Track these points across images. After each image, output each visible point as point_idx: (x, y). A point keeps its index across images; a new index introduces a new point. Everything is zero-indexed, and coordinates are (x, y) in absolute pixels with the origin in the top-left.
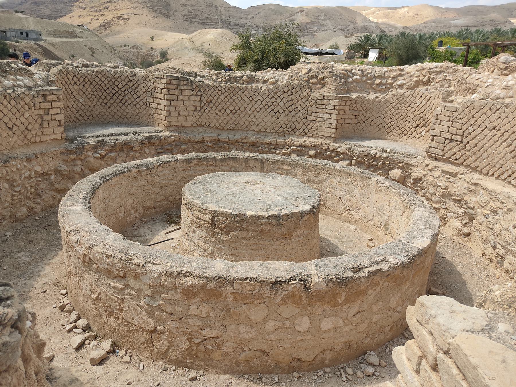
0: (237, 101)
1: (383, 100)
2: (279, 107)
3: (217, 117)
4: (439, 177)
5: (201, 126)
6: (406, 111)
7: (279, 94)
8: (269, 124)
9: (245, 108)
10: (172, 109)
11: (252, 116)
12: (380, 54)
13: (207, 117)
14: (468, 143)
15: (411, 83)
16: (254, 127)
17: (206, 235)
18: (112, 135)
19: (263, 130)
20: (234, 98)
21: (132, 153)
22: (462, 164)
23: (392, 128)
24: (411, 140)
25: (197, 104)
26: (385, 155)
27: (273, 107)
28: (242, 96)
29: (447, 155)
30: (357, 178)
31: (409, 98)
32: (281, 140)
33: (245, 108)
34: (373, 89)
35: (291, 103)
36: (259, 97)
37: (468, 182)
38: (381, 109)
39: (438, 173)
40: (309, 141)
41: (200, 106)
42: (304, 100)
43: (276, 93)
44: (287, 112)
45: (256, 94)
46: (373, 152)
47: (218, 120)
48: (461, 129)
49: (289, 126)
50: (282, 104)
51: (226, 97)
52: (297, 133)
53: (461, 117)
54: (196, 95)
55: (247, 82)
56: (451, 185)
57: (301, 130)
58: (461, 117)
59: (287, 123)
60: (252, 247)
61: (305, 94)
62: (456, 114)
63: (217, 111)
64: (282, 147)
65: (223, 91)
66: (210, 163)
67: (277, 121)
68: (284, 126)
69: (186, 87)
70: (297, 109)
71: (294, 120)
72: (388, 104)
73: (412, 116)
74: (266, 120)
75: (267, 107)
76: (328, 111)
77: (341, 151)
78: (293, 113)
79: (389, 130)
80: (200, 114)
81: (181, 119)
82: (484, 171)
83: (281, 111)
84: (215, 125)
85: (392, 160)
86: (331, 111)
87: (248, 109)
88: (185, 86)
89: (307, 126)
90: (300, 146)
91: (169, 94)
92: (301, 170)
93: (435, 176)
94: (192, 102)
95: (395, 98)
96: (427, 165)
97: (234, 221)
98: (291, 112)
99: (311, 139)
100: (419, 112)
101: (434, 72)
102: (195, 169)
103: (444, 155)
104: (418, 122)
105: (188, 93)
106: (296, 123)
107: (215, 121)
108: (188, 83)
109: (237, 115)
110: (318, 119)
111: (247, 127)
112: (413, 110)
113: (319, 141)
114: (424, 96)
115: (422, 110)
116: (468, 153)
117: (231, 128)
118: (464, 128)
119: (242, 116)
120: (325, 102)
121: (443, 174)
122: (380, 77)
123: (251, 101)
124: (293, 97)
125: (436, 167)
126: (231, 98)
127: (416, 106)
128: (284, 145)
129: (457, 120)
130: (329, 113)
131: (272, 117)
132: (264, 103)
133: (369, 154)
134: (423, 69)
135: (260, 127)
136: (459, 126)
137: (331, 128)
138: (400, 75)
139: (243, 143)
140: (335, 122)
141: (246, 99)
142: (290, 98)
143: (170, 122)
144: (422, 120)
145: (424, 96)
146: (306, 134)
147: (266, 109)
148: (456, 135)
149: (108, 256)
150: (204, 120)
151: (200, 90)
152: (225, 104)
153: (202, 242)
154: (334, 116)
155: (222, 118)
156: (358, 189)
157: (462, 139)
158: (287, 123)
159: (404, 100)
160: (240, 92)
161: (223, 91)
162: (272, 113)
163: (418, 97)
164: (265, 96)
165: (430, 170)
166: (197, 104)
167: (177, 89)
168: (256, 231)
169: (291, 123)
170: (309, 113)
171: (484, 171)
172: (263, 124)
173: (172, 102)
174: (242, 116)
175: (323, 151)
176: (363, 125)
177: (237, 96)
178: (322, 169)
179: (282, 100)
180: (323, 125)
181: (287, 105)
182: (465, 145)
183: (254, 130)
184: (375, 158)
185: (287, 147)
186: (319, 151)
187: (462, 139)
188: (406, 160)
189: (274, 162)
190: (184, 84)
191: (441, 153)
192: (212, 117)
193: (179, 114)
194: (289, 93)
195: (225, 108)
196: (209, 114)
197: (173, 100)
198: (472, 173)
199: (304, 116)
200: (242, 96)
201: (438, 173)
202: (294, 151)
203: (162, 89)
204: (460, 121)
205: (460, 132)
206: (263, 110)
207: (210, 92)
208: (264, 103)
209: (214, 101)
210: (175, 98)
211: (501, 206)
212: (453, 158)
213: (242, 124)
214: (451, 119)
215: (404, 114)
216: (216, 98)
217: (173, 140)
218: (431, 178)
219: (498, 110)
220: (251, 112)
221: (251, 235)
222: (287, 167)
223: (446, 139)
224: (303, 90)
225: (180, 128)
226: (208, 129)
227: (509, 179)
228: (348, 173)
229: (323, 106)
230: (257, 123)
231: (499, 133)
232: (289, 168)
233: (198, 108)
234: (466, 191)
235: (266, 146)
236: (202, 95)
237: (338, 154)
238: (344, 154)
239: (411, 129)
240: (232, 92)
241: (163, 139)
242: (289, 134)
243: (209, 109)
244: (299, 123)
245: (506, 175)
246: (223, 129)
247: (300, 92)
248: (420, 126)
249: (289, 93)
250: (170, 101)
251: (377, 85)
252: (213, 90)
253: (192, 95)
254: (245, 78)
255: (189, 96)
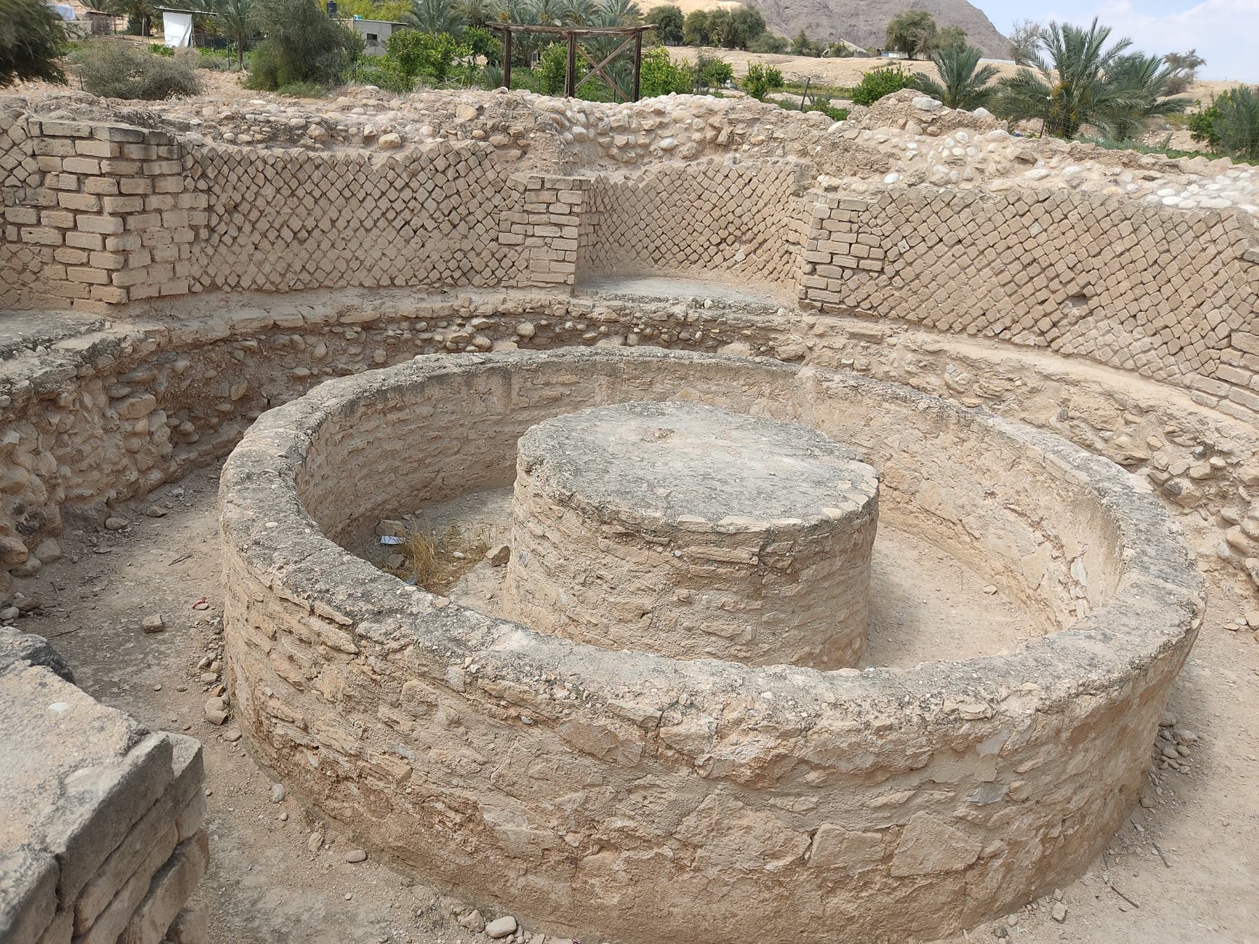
0: (309, 201)
1: (641, 186)
2: (424, 214)
3: (258, 256)
4: (844, 346)
5: (214, 287)
6: (693, 210)
7: (422, 177)
8: (400, 262)
9: (333, 222)
10: (132, 242)
11: (353, 245)
12: (197, 28)
13: (231, 259)
14: (897, 273)
15: (689, 144)
16: (362, 275)
17: (735, 598)
18: (1063, 380)
19: (385, 281)
20: (300, 193)
21: (55, 420)
22: (886, 316)
23: (663, 249)
24: (710, 273)
25: (200, 218)
26: (707, 314)
27: (407, 215)
28: (324, 185)
29: (850, 302)
30: (758, 378)
31: (699, 180)
32: (436, 304)
33: (333, 222)
34: (613, 157)
35: (455, 200)
36: (368, 187)
37: (915, 350)
38: (639, 206)
39: (839, 341)
40: (513, 299)
41: (207, 226)
42: (489, 192)
43: (414, 175)
44: (446, 227)
45: (362, 178)
46: (678, 310)
47: (260, 265)
48: (880, 246)
49: (453, 265)
50: (431, 205)
51: (278, 191)
52: (477, 280)
53: (879, 221)
54: (196, 189)
55: (323, 143)
56: (874, 360)
57: (487, 272)
58: (879, 221)
59: (447, 255)
60: (836, 592)
61: (491, 175)
62: (865, 217)
63: (256, 237)
64: (445, 324)
65: (270, 172)
66: (391, 404)
67: (423, 253)
68: (441, 266)
69: (165, 167)
70: (471, 217)
71: (466, 247)
72: (652, 194)
73: (708, 220)
74: (391, 252)
75: (391, 215)
76: (554, 219)
77: (602, 317)
78: (463, 227)
79: (657, 255)
80: (210, 251)
81: (160, 274)
82: (942, 325)
83: (430, 225)
84: (254, 282)
85: (725, 323)
86: (563, 220)
87: (341, 224)
88: (164, 163)
89: (500, 261)
90: (495, 314)
91: (121, 194)
92: (603, 380)
93: (836, 346)
94: (185, 214)
95: (666, 180)
96: (812, 327)
97: (811, 542)
98: (455, 226)
99: (513, 294)
100: (724, 211)
101: (742, 121)
102: (362, 429)
103: (842, 302)
104: (723, 233)
105: (171, 185)
106: (471, 255)
107: (252, 269)
108: (170, 151)
109: (311, 245)
110: (529, 241)
111: (341, 277)
112: (708, 206)
113: (537, 297)
114: (733, 175)
115: (732, 205)
116: (897, 294)
117: (300, 286)
118: (887, 244)
119: (326, 245)
120: (547, 196)
121: (855, 341)
122: (623, 129)
123: (347, 199)
124: (461, 184)
125: (832, 328)
126: (293, 194)
127: (714, 199)
128: (451, 317)
129: (868, 230)
130: (555, 225)
131: (407, 241)
132: (384, 204)
133: (670, 316)
134: (711, 112)
135: (377, 272)
136: (875, 241)
137: (564, 261)
138: (662, 126)
139: (342, 325)
140: (574, 245)
141: (333, 194)
142: (453, 187)
143: (128, 289)
144: (731, 228)
145: (733, 175)
146: (499, 281)
147: (390, 222)
148: (868, 258)
149: (879, 731)
150: (220, 272)
151: (204, 175)
152: (278, 212)
153: (721, 622)
154: (572, 232)
155: (272, 258)
156: (763, 401)
157: (884, 265)
158: (447, 255)
159: (686, 185)
160: (317, 175)
161: (270, 172)
162: (407, 231)
163: (719, 178)
164: (384, 185)
165: (821, 336)
166: (200, 218)
167: (141, 173)
168: (846, 552)
169: (459, 255)
170: (503, 226)
171: (942, 325)
172: (385, 264)
173: (131, 220)
174: (326, 245)
175: (553, 321)
176: (607, 246)
177: (309, 186)
178: (659, 369)
179: (430, 193)
180: (545, 256)
181: (446, 207)
182: (891, 279)
183: (361, 284)
184: (684, 324)
185: (459, 321)
186: (544, 322)
187: (884, 265)
188: (759, 320)
189: (535, 371)
190: (159, 158)
191: (836, 298)
192: (244, 257)
193: (153, 260)
194: (451, 173)
195: (277, 225)
196: (236, 248)
197: (131, 214)
198: (910, 332)
199: (493, 234)
200: (324, 185)
201: (839, 341)
202: (479, 329)
203: (82, 177)
204: (877, 231)
205: (879, 253)
206: (382, 223)
207: (233, 178)
208: (384, 204)
209: (245, 207)
210: (137, 204)
211: (1008, 385)
212: (865, 305)
213: (328, 268)
214: (855, 227)
215: (688, 217)
216: (250, 196)
217: (153, 347)
218: (829, 353)
219: (968, 206)
220: (349, 232)
221: (838, 563)
222: (569, 378)
223: (843, 268)
224: (487, 164)
225: (157, 303)
226: (235, 297)
227: (1007, 335)
228: (730, 369)
229: (543, 208)
230: (367, 264)
231: (973, 251)
232: (574, 378)
233: (204, 233)
234: (912, 369)
235: (405, 325)
236: (210, 189)
237: (593, 324)
238: (610, 322)
239: (706, 249)
240: (294, 176)
241: (130, 350)
242: (455, 285)
243: (234, 232)
244: (478, 255)
245: (998, 327)
246: (278, 291)
247: (478, 172)
248: (729, 241)
249: (451, 173)
250: (124, 216)
251: (619, 148)
252: (240, 170)
253: (185, 190)
254: (315, 130)
255: (175, 195)
